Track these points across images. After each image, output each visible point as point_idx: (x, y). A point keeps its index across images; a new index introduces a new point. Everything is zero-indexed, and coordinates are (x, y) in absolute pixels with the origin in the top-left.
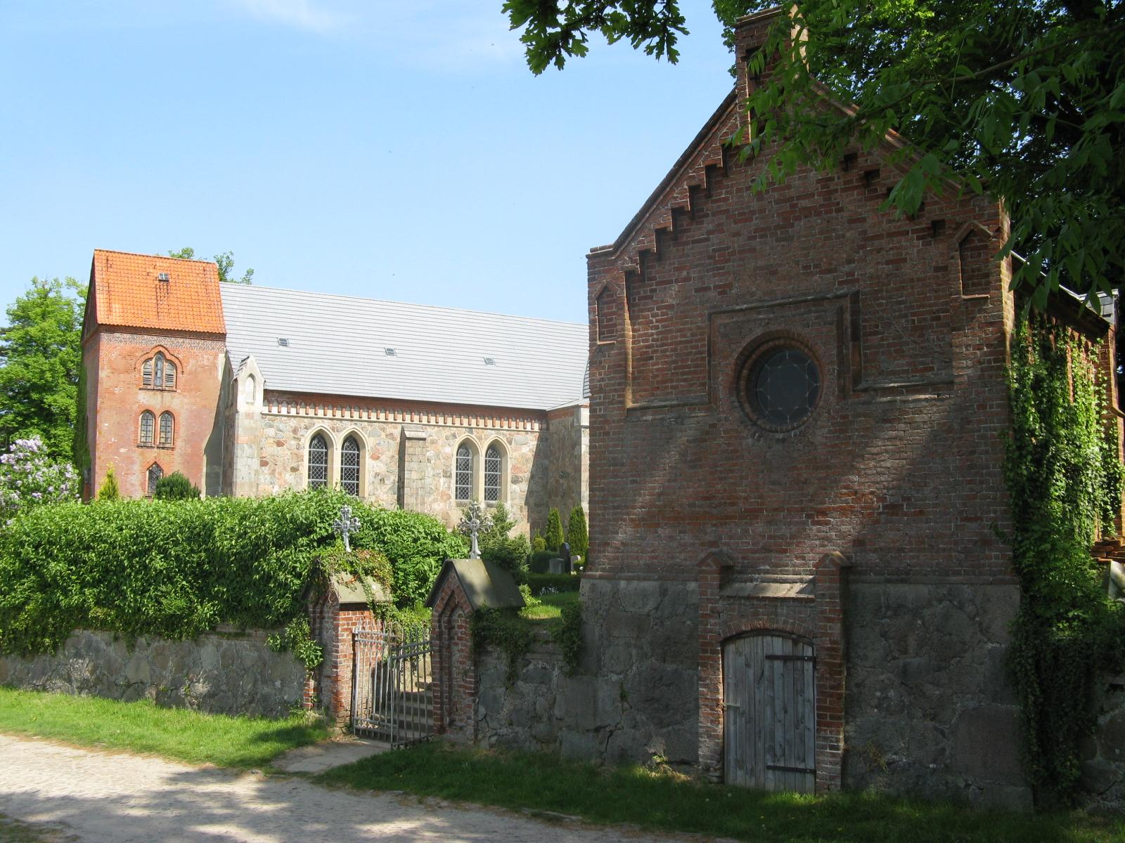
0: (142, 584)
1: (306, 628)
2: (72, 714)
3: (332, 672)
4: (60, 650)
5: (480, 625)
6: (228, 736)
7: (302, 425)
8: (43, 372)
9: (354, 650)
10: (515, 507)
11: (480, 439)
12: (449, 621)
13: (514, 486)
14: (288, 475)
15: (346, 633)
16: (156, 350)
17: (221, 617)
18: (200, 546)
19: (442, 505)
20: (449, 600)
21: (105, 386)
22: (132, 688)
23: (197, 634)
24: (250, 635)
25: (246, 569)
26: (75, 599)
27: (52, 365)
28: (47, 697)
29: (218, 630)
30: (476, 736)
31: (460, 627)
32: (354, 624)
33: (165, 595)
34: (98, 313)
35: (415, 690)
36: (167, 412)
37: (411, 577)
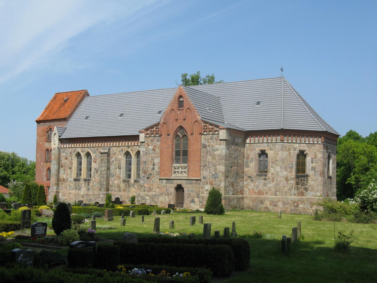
11: (132, 150)
19: (117, 181)
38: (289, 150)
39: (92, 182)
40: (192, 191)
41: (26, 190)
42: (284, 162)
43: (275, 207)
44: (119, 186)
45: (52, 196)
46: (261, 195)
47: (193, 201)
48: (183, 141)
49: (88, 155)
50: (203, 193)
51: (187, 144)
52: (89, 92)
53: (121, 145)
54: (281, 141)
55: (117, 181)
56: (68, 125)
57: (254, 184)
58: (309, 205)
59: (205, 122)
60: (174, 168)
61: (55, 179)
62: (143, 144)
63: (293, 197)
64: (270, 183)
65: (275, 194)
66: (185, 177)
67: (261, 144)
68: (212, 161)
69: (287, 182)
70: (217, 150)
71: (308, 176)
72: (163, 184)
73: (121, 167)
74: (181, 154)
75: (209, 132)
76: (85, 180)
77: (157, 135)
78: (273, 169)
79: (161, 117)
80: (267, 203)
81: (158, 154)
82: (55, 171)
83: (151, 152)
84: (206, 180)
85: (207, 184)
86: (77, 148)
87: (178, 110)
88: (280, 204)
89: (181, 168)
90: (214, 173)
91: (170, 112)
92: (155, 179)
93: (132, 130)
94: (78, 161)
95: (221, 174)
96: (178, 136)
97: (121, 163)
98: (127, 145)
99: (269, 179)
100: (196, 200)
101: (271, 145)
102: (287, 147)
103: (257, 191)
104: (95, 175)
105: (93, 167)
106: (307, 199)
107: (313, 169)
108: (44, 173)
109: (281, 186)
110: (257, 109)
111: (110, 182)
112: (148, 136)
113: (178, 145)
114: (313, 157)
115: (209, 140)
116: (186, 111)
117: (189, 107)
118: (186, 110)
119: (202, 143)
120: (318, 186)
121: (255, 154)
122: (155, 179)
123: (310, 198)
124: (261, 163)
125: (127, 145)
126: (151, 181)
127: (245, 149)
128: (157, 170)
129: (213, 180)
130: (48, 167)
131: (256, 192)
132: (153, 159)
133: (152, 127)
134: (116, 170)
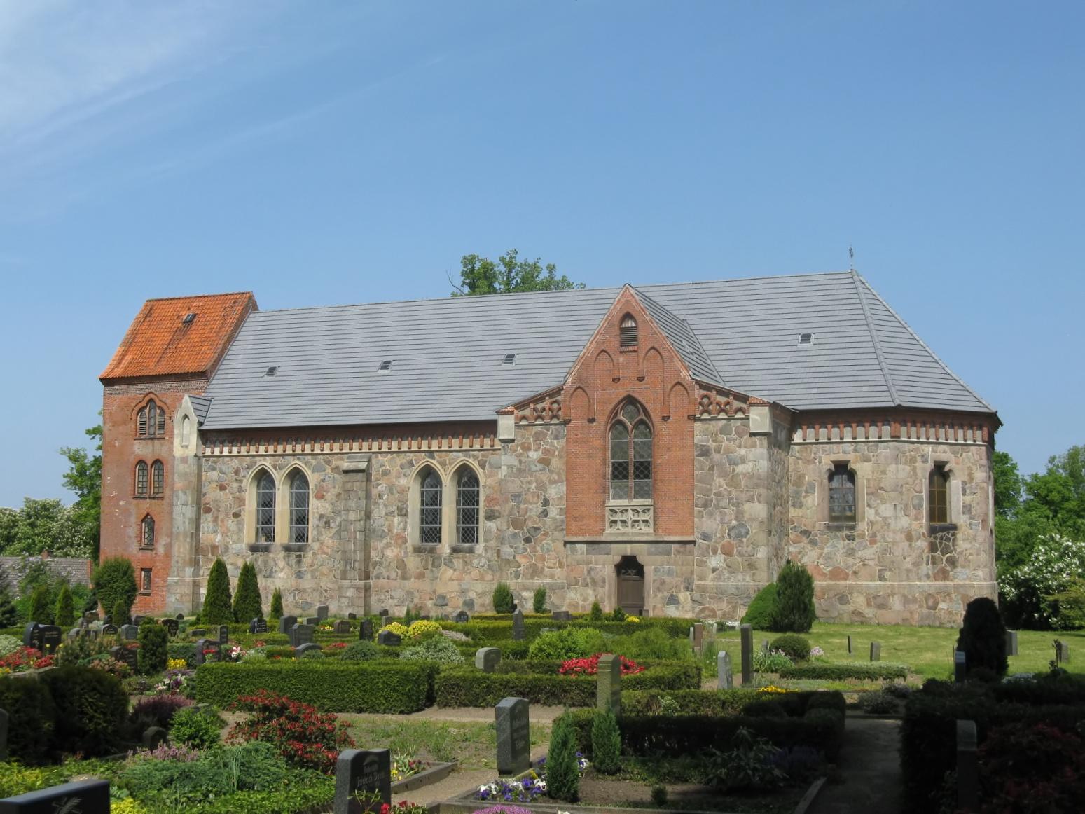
7: (244, 465)
10: (489, 551)
11: (443, 464)
13: (489, 524)
14: (230, 523)
19: (396, 551)
38: (913, 460)
39: (310, 554)
40: (670, 573)
41: (217, 580)
42: (901, 493)
43: (880, 612)
44: (401, 565)
45: (178, 596)
46: (839, 580)
47: (673, 600)
48: (635, 437)
49: (296, 477)
50: (701, 578)
51: (650, 446)
52: (257, 298)
53: (407, 450)
54: (892, 437)
55: (395, 550)
56: (211, 391)
57: (817, 550)
58: (960, 602)
59: (703, 386)
60: (612, 510)
61: (187, 547)
62: (510, 445)
63: (925, 583)
64: (865, 547)
65: (880, 577)
66: (647, 534)
67: (835, 446)
68: (729, 492)
69: (910, 545)
70: (743, 460)
71: (954, 527)
72: (579, 556)
73: (407, 511)
74: (634, 471)
75: (719, 414)
76: (287, 549)
77: (555, 421)
78: (873, 511)
79: (567, 370)
80: (859, 602)
81: (558, 474)
82: (187, 523)
83: (534, 468)
84: (712, 543)
85: (715, 552)
86: (257, 458)
87: (621, 352)
88: (896, 603)
89: (633, 510)
90: (734, 523)
91: (596, 358)
92: (552, 544)
93: (317, 411)
94: (258, 494)
95: (755, 524)
96: (620, 422)
97: (407, 501)
98: (425, 448)
99: (862, 536)
100: (683, 596)
101: (864, 448)
102: (908, 454)
103: (829, 569)
104: (320, 534)
105: (315, 511)
106: (957, 587)
107: (967, 509)
108: (132, 531)
109: (896, 554)
110: (808, 353)
111: (373, 554)
112: (524, 422)
113: (618, 449)
114: (966, 478)
115: (716, 435)
116: (645, 357)
117: (656, 346)
118: (647, 353)
119: (696, 442)
120: (978, 554)
121: (820, 472)
122: (552, 544)
123: (963, 586)
124: (835, 496)
125: (427, 449)
126: (538, 548)
127: (791, 460)
128: (558, 517)
129: (732, 542)
130: (145, 513)
131: (825, 571)
132: (542, 486)
133: (539, 399)
134: (389, 518)
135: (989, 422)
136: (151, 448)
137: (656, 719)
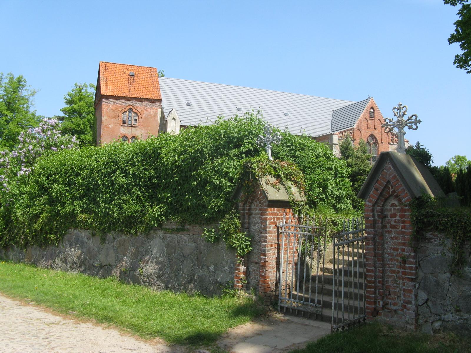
0: (110, 196)
1: (238, 223)
2: (62, 286)
3: (260, 259)
4: (61, 243)
5: (423, 212)
6: (173, 311)
8: (80, 125)
9: (278, 240)
12: (382, 211)
15: (272, 226)
16: (128, 108)
17: (166, 217)
18: (150, 166)
20: (383, 190)
21: (104, 124)
22: (103, 268)
23: (149, 230)
24: (188, 230)
25: (186, 179)
26: (68, 209)
27: (84, 121)
28: (52, 273)
29: (164, 227)
30: (417, 320)
31: (394, 216)
32: (278, 219)
33: (125, 202)
34: (101, 90)
35: (321, 273)
36: (134, 137)
37: (316, 185)
135: (467, 73)
136: (130, 131)
137: (283, 314)
